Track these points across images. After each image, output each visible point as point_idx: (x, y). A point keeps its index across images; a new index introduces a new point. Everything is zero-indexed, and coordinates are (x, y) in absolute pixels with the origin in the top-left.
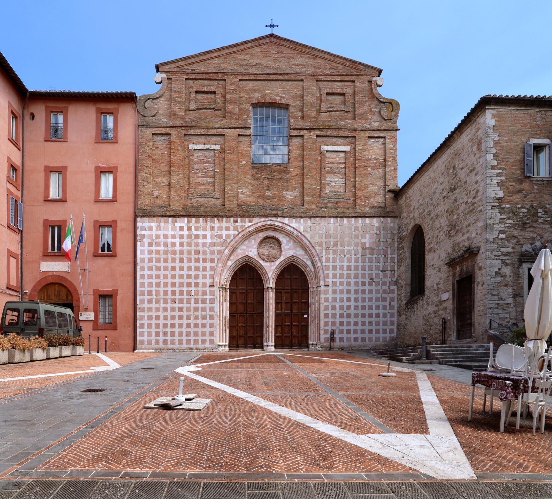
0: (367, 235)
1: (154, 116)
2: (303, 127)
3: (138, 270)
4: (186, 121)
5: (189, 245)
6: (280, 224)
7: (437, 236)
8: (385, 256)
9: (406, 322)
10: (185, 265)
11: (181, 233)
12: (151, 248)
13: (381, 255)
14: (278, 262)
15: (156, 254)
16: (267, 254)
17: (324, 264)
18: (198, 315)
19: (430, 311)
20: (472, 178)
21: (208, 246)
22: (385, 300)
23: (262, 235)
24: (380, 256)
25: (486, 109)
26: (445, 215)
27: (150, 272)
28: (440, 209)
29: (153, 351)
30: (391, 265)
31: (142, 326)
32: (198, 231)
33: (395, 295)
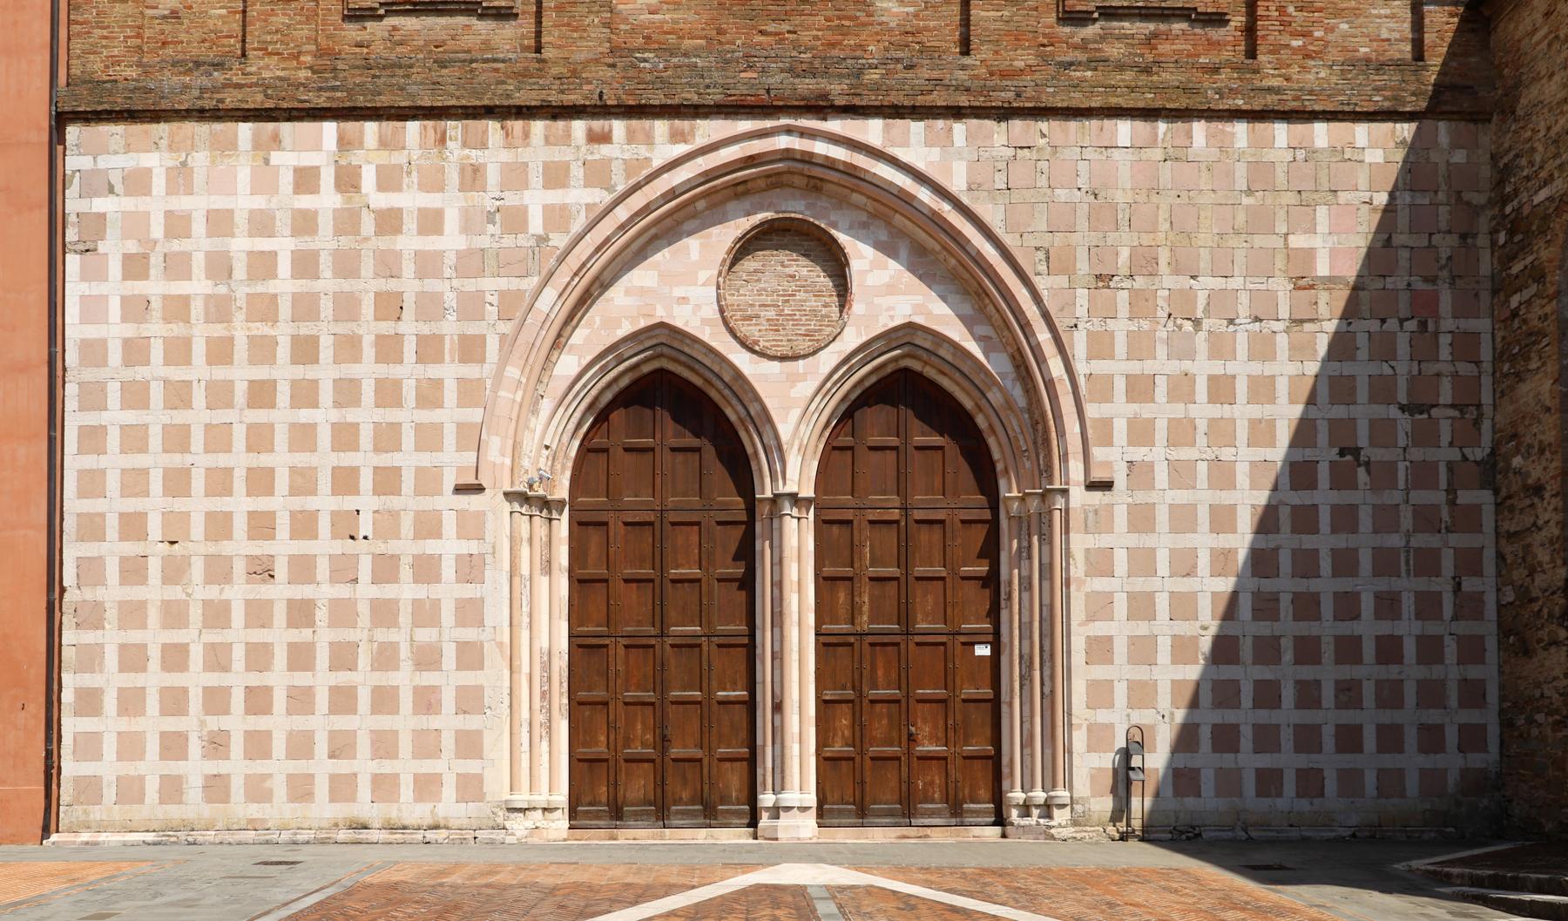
0: (1322, 212)
3: (71, 404)
5: (346, 266)
8: (1423, 325)
10: (325, 372)
12: (138, 287)
14: (828, 359)
15: (167, 320)
16: (771, 313)
18: (394, 646)
21: (448, 272)
22: (1427, 563)
24: (1392, 324)
30: (1455, 375)
32: (398, 188)
33: (1485, 540)
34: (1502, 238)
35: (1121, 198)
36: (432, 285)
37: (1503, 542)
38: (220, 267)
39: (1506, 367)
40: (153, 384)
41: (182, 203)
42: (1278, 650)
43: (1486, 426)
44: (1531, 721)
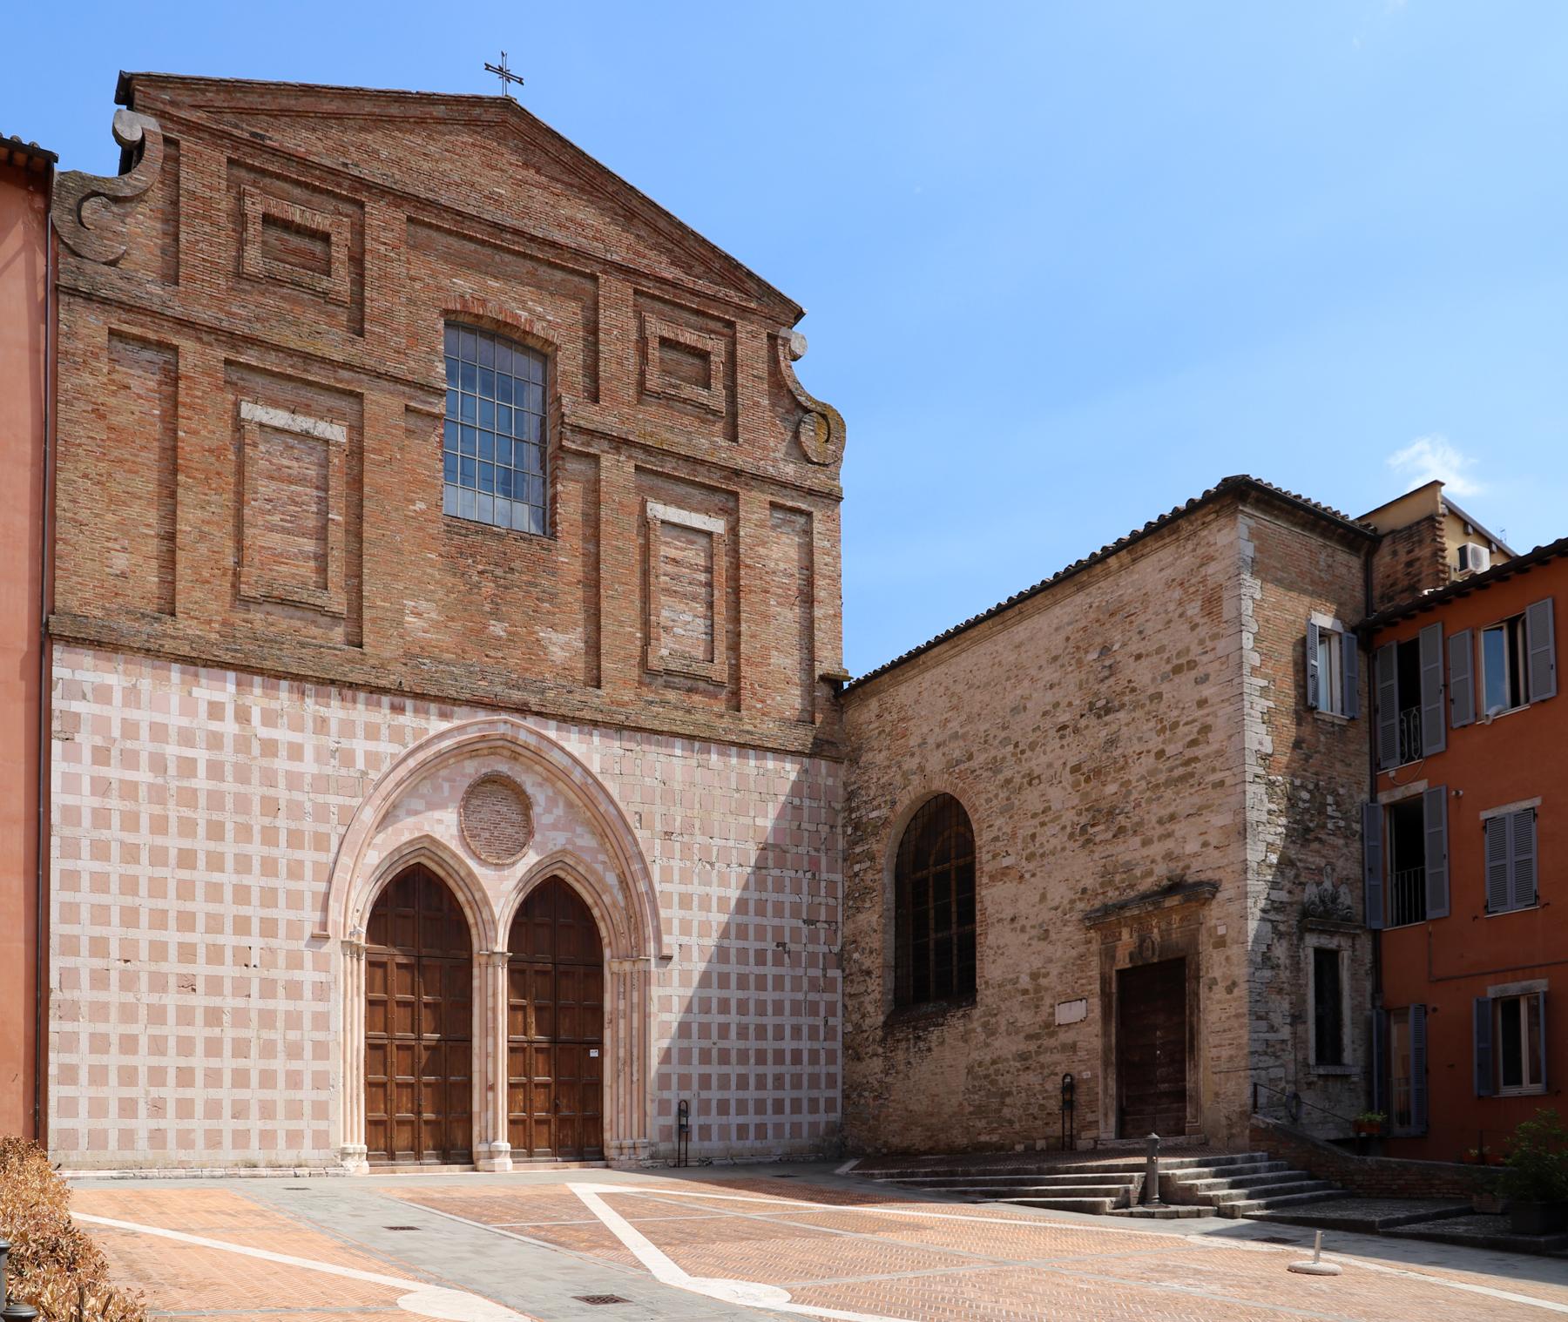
1: (113, 263)
2: (601, 428)
3: (55, 852)
4: (229, 313)
5: (242, 776)
6: (532, 741)
7: (1033, 836)
8: (814, 875)
9: (889, 1079)
10: (229, 848)
11: (215, 726)
12: (103, 771)
13: (805, 872)
14: (461, 852)
15: (122, 798)
16: (487, 835)
17: (658, 888)
19: (999, 1053)
20: (1184, 689)
21: (307, 788)
22: (813, 1009)
23: (473, 769)
24: (800, 873)
25: (1236, 511)
26: (1068, 778)
27: (97, 866)
28: (1044, 759)
29: (114, 1173)
30: (827, 905)
31: (69, 1074)
32: (275, 726)
33: (838, 997)
34: (849, 831)
35: (677, 787)
36: (297, 796)
37: (846, 999)
38: (158, 764)
39: (851, 903)
40: (113, 843)
41: (133, 714)
42: (748, 1056)
43: (839, 933)
44: (860, 1095)
